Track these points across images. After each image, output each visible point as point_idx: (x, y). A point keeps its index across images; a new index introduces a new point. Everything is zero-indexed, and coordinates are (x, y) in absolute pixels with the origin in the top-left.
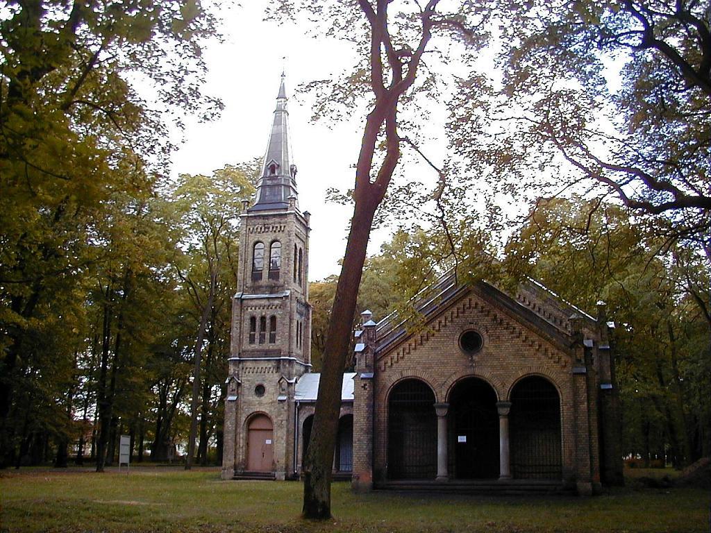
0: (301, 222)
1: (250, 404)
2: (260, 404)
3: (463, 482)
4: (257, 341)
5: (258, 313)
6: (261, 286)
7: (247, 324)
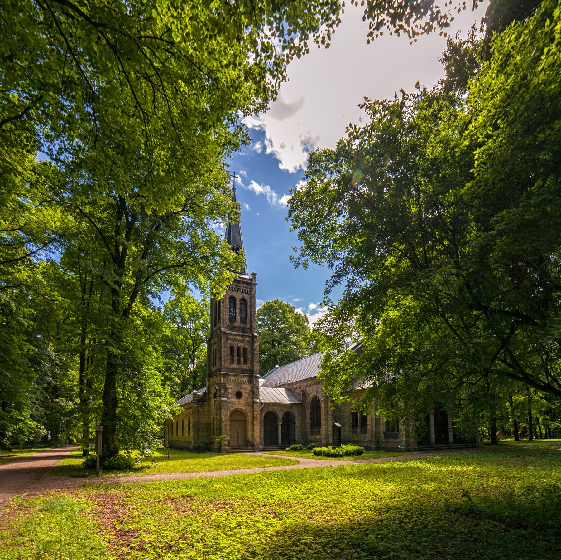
0: (384, 472)
1: (233, 403)
2: (239, 403)
3: (396, 465)
4: (235, 362)
5: (235, 344)
6: (236, 327)
7: (227, 351)
